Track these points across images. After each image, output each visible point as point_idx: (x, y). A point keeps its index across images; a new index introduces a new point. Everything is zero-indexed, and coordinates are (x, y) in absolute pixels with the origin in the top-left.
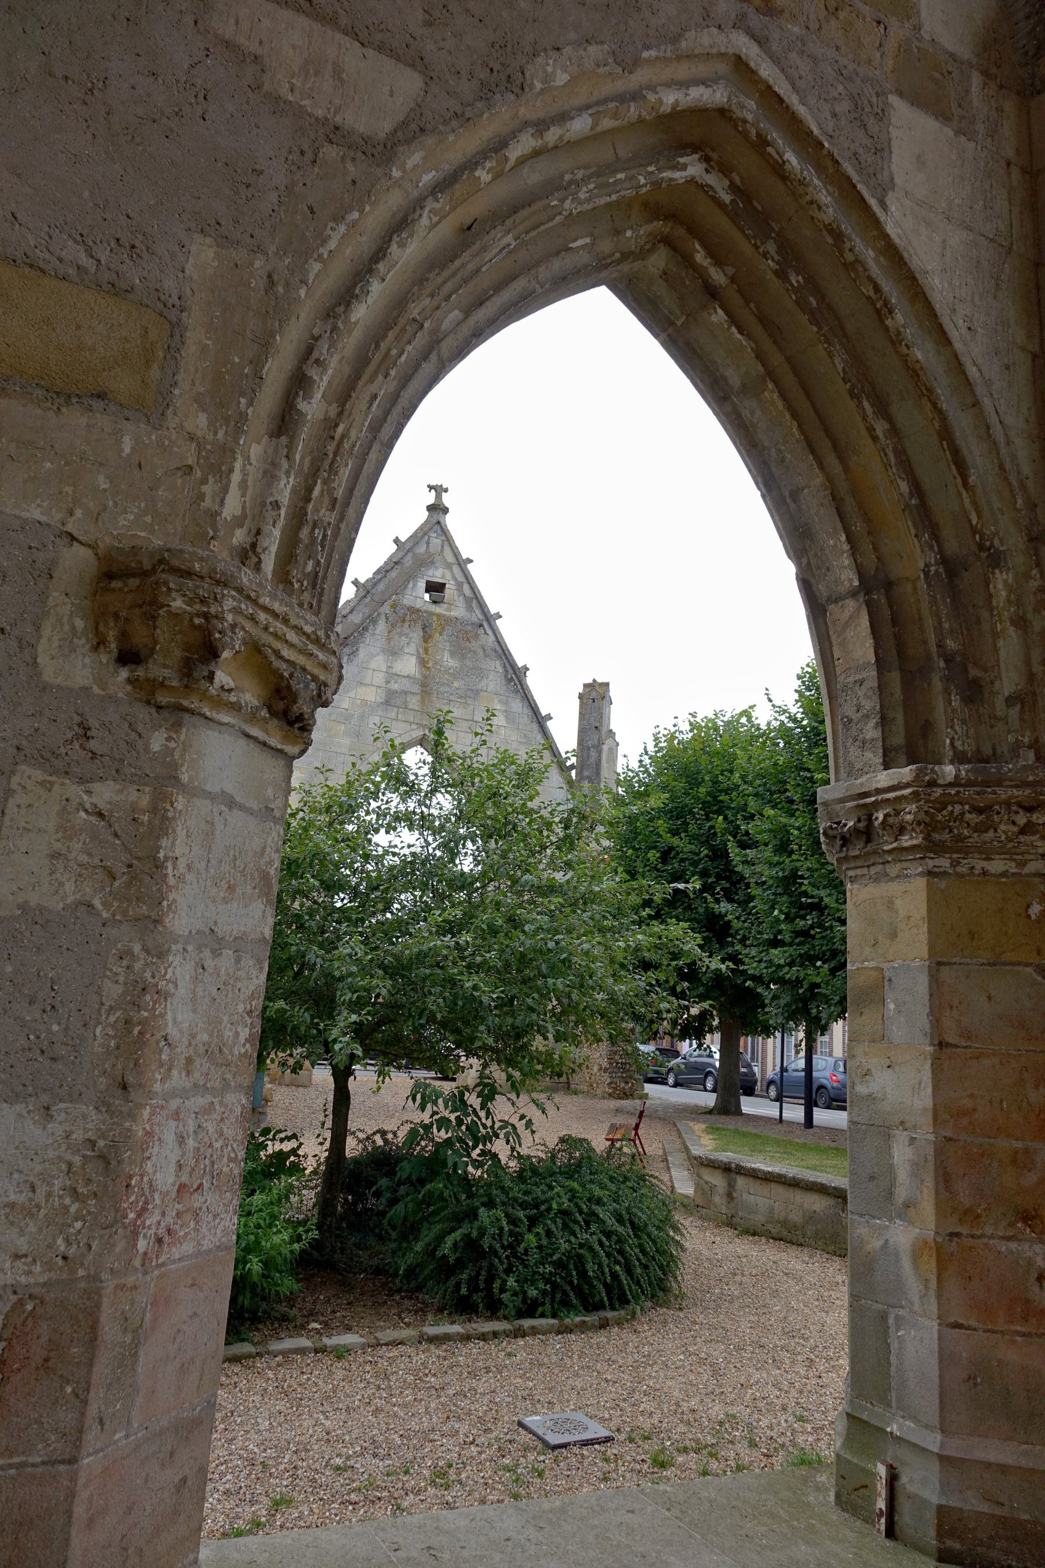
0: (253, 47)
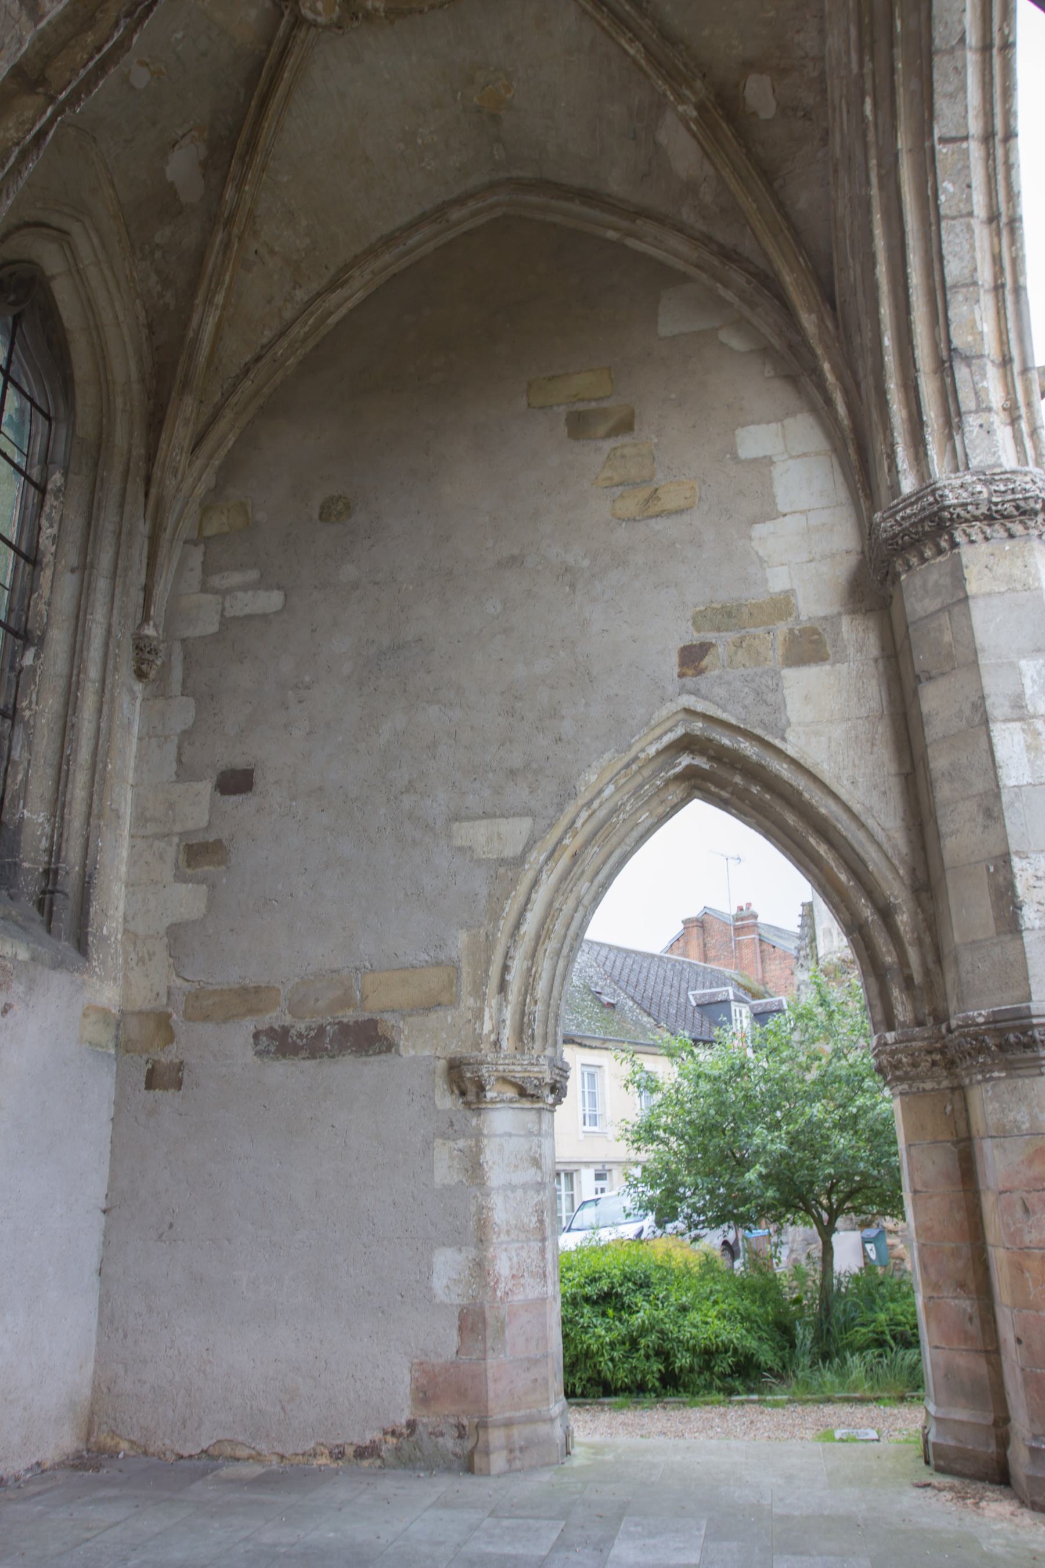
0: (467, 844)
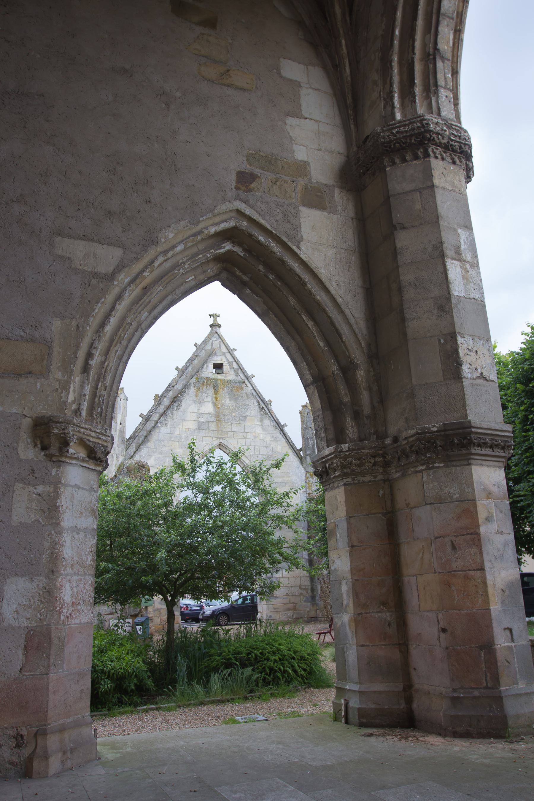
0: (68, 255)
